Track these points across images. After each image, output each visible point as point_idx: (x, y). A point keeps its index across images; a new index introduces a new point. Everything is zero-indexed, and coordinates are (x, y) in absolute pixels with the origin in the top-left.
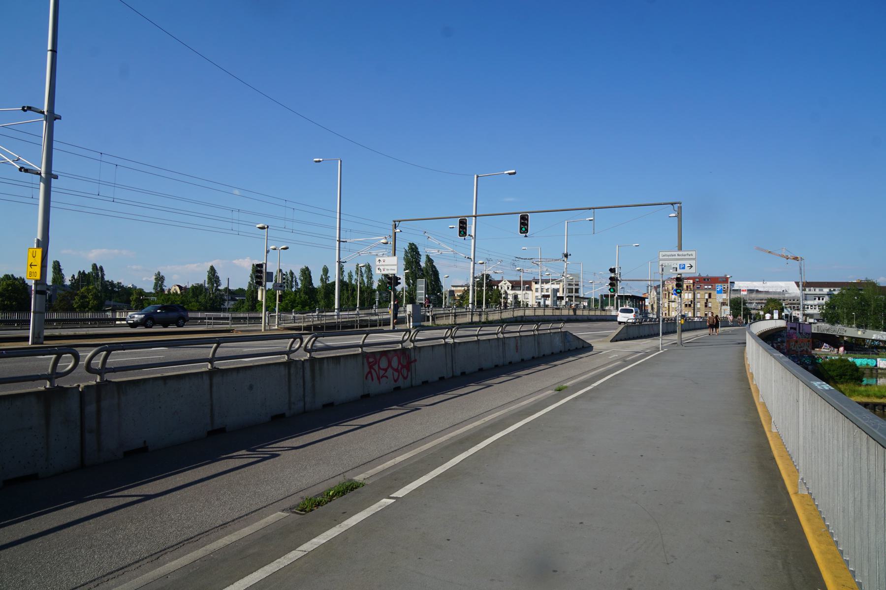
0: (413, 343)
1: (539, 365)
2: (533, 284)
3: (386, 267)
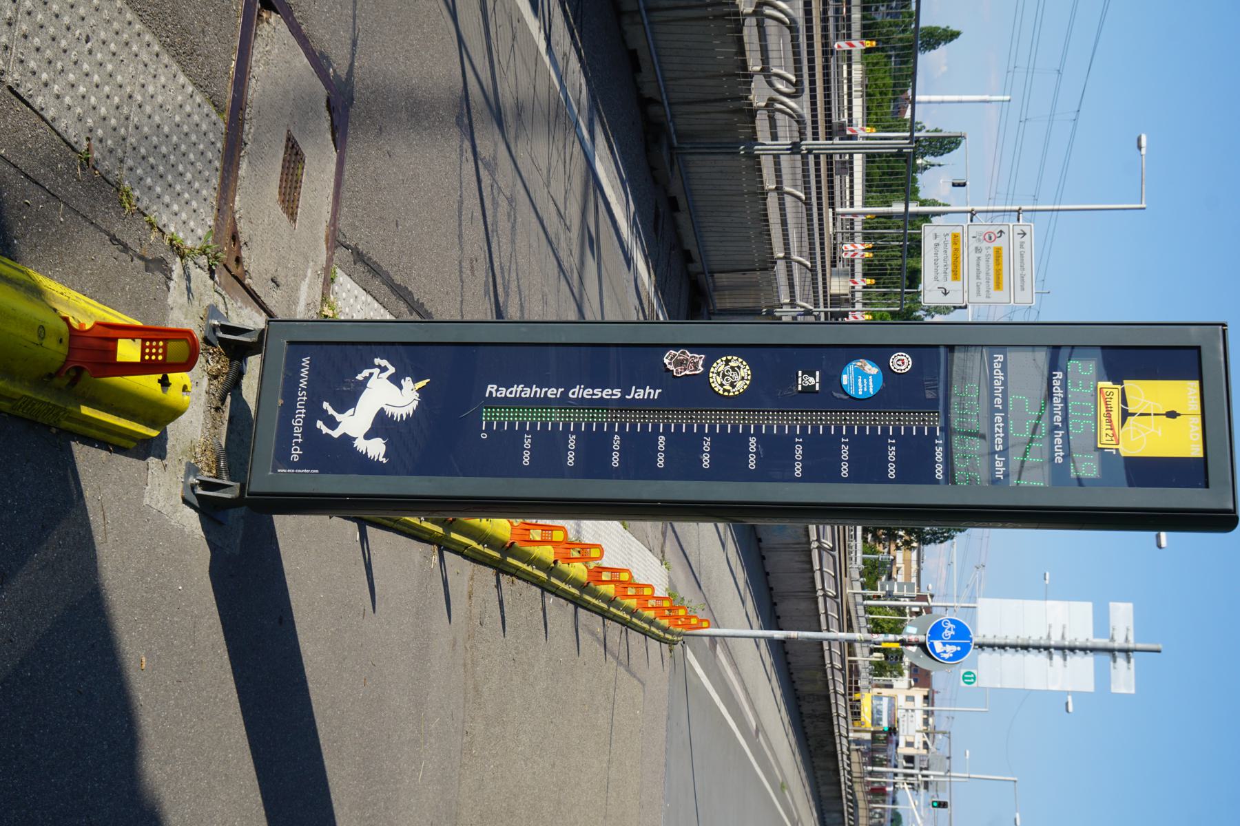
0: (755, 13)
1: (651, 257)
2: (925, 691)
3: (906, 724)
